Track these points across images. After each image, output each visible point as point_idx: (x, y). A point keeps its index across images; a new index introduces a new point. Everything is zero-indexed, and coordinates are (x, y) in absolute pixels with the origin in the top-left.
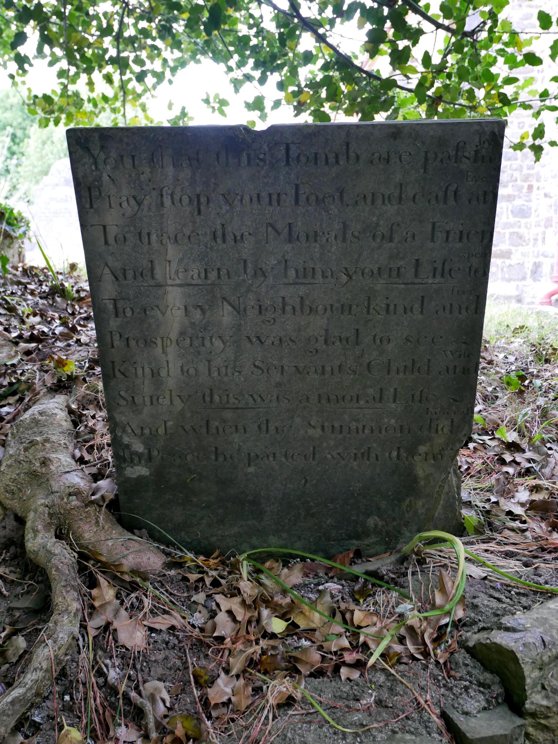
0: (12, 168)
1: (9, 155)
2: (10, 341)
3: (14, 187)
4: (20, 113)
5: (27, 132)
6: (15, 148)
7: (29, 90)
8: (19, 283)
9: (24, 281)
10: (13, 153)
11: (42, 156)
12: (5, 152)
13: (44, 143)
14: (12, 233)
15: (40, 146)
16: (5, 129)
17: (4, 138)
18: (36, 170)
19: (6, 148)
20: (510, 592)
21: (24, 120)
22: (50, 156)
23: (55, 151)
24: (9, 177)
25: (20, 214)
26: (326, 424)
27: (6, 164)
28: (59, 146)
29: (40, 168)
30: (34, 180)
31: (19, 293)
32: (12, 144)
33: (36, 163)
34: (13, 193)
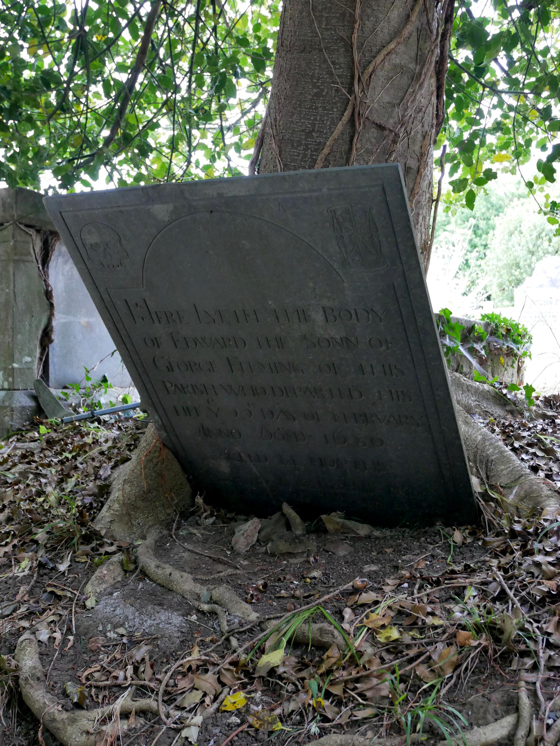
0: (472, 262)
1: (469, 249)
2: (555, 491)
3: (473, 282)
4: (485, 203)
5: (491, 222)
6: (477, 240)
7: (547, 197)
8: (544, 417)
9: (550, 413)
10: (474, 246)
11: (508, 248)
12: (467, 246)
13: (511, 234)
14: (516, 351)
15: (507, 237)
16: (468, 221)
17: (466, 231)
18: (500, 264)
19: (467, 241)
20: (76, 468)
21: (488, 209)
22: (517, 247)
23: (523, 242)
24: (468, 272)
25: (525, 330)
26: (393, 390)
27: (466, 257)
28: (528, 236)
29: (505, 262)
30: (497, 273)
31: (550, 430)
32: (474, 236)
33: (501, 257)
34: (472, 289)
